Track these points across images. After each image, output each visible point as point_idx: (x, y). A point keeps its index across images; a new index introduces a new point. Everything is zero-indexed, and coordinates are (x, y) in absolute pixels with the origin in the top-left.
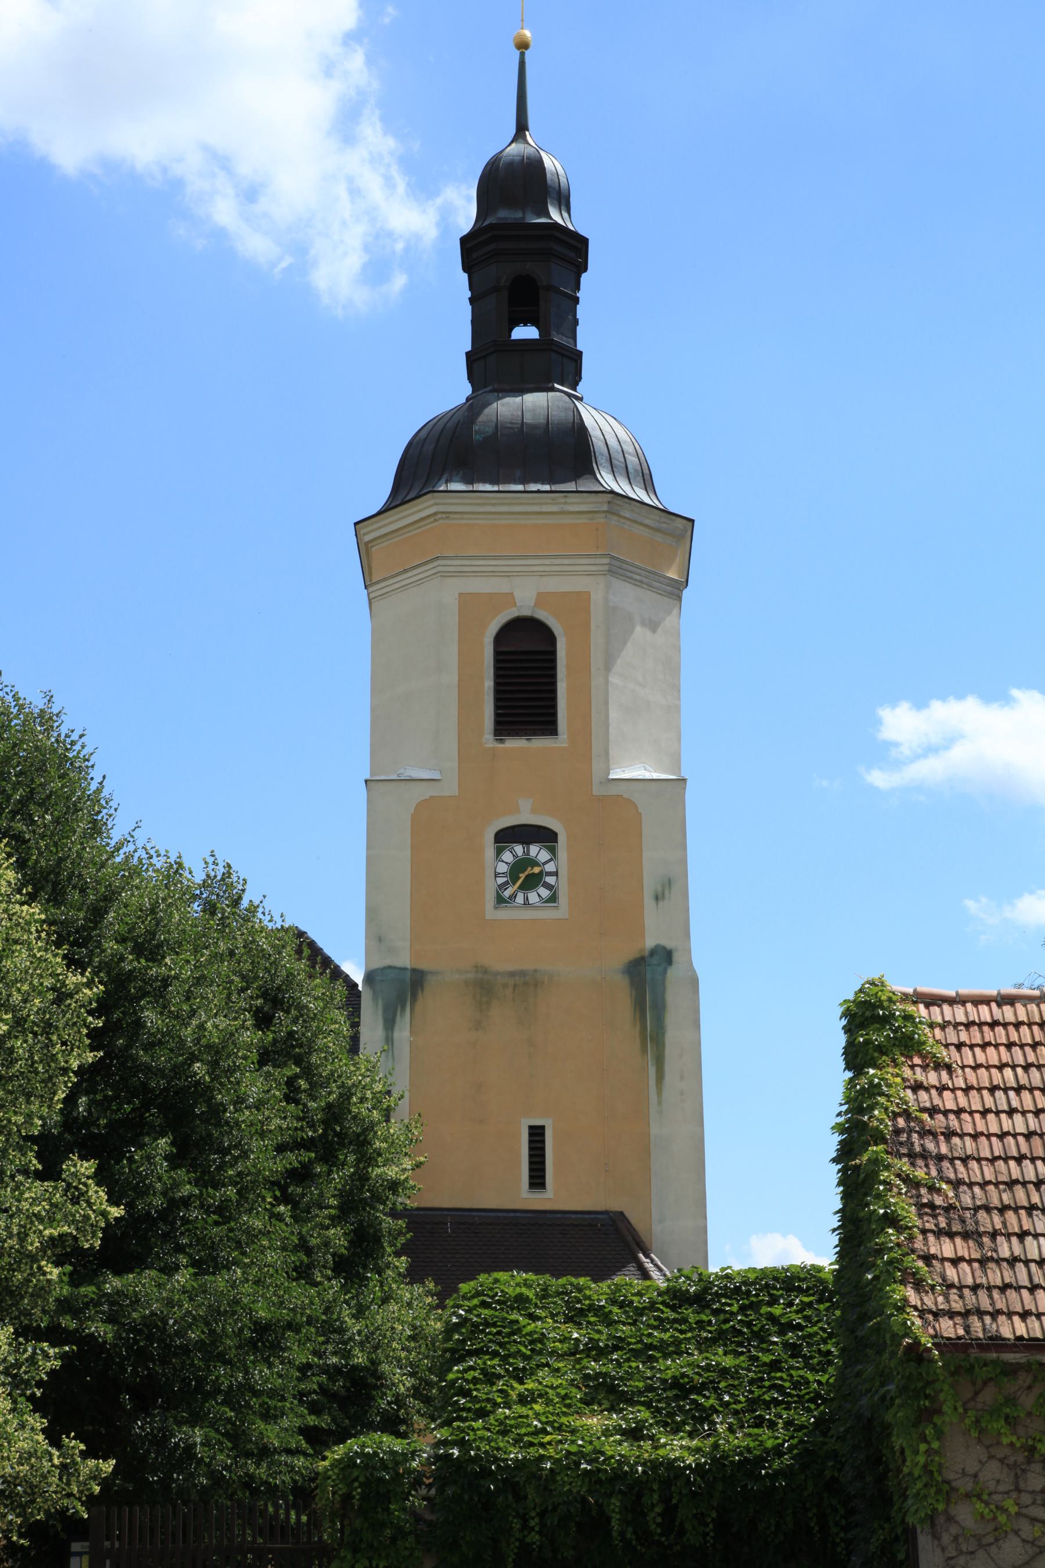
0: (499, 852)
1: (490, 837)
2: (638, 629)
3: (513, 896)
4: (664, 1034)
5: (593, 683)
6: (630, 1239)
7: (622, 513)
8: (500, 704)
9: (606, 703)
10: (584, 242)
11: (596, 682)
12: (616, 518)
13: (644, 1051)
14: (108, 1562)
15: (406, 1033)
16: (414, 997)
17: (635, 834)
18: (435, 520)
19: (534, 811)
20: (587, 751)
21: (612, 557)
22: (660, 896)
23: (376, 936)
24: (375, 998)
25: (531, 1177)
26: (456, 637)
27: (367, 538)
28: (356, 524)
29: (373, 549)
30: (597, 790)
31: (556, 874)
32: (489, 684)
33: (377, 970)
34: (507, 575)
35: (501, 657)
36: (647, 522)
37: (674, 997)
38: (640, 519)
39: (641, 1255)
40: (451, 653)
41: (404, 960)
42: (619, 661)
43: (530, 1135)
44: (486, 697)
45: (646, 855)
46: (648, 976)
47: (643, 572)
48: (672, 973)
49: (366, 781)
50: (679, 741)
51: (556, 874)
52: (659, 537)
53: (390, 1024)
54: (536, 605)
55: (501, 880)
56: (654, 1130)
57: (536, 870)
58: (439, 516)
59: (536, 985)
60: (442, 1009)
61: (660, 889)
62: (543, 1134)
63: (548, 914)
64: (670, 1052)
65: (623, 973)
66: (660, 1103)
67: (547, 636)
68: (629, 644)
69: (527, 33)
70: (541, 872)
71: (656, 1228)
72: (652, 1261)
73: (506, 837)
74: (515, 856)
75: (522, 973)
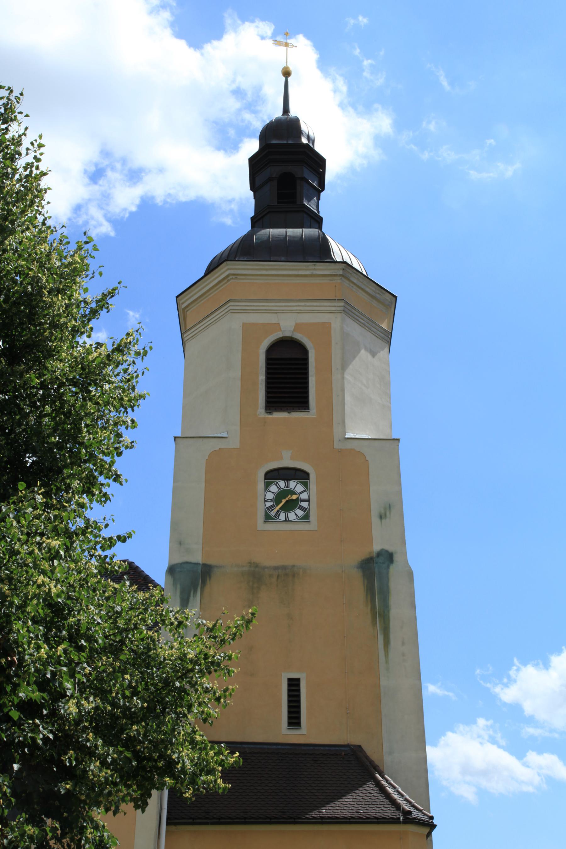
0: (268, 485)
2: (363, 351)
3: (278, 514)
4: (389, 611)
5: (334, 378)
6: (368, 763)
7: (352, 279)
8: (270, 371)
9: (343, 390)
10: (322, 218)
11: (336, 376)
12: (347, 282)
13: (374, 623)
16: (204, 583)
17: (365, 476)
18: (228, 281)
19: (292, 458)
20: (330, 419)
21: (346, 302)
22: (383, 516)
23: (178, 541)
25: (289, 718)
26: (240, 349)
27: (184, 306)
28: (177, 297)
29: (188, 313)
30: (337, 445)
31: (308, 500)
32: (262, 377)
33: (177, 565)
34: (276, 312)
35: (270, 371)
36: (367, 289)
37: (395, 583)
38: (363, 287)
39: (378, 775)
40: (237, 358)
41: (197, 558)
42: (351, 366)
43: (289, 685)
44: (260, 386)
45: (373, 488)
46: (376, 570)
47: (365, 319)
48: (393, 569)
49: (175, 438)
50: (391, 428)
51: (308, 500)
54: (294, 330)
55: (268, 504)
56: (384, 682)
57: (294, 497)
58: (231, 277)
59: (294, 576)
61: (383, 512)
62: (299, 685)
63: (303, 527)
64: (394, 624)
65: (358, 568)
66: (387, 662)
67: (304, 351)
68: (357, 359)
70: (298, 499)
72: (387, 781)
73: (272, 476)
74: (279, 488)
75: (284, 568)
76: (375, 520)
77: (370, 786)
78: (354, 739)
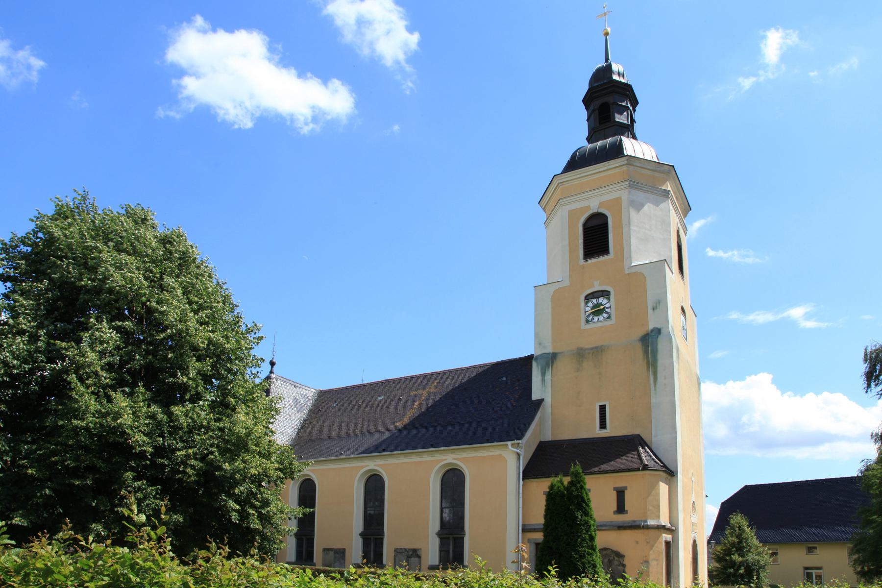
0: (586, 303)
1: (583, 298)
3: (593, 319)
11: (625, 230)
14: (711, 253)
15: (550, 377)
16: (553, 363)
17: (643, 287)
20: (622, 256)
24: (538, 365)
30: (627, 271)
34: (587, 199)
41: (549, 350)
52: (657, 174)
53: (543, 374)
56: (653, 401)
60: (564, 366)
63: (608, 323)
69: (609, 30)
71: (654, 439)
73: (588, 298)
75: (596, 348)
76: (650, 311)
77: (634, 453)
78: (636, 432)
